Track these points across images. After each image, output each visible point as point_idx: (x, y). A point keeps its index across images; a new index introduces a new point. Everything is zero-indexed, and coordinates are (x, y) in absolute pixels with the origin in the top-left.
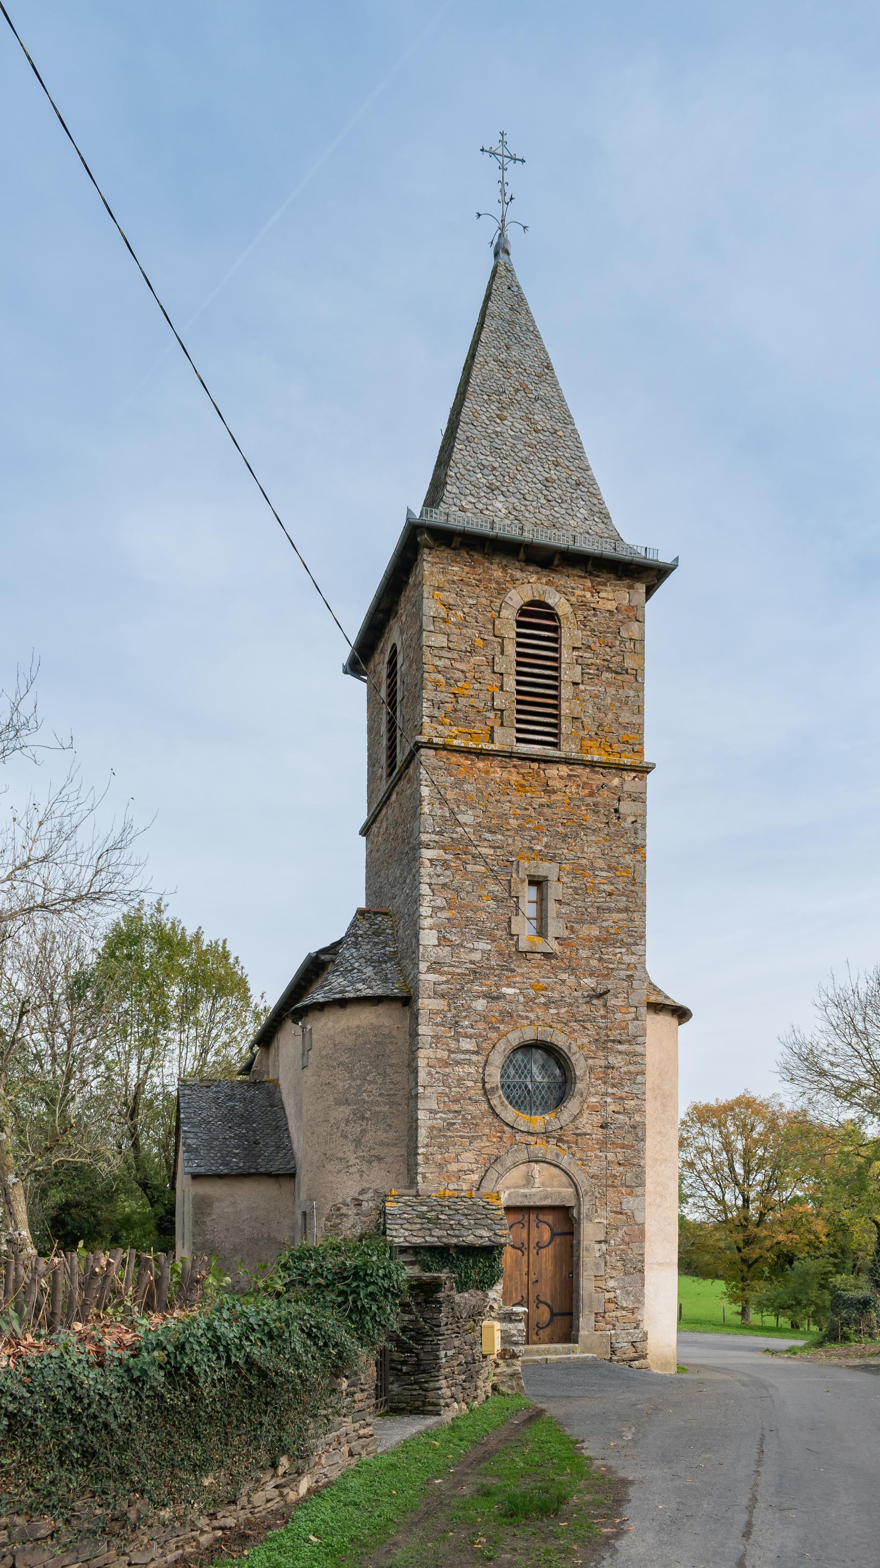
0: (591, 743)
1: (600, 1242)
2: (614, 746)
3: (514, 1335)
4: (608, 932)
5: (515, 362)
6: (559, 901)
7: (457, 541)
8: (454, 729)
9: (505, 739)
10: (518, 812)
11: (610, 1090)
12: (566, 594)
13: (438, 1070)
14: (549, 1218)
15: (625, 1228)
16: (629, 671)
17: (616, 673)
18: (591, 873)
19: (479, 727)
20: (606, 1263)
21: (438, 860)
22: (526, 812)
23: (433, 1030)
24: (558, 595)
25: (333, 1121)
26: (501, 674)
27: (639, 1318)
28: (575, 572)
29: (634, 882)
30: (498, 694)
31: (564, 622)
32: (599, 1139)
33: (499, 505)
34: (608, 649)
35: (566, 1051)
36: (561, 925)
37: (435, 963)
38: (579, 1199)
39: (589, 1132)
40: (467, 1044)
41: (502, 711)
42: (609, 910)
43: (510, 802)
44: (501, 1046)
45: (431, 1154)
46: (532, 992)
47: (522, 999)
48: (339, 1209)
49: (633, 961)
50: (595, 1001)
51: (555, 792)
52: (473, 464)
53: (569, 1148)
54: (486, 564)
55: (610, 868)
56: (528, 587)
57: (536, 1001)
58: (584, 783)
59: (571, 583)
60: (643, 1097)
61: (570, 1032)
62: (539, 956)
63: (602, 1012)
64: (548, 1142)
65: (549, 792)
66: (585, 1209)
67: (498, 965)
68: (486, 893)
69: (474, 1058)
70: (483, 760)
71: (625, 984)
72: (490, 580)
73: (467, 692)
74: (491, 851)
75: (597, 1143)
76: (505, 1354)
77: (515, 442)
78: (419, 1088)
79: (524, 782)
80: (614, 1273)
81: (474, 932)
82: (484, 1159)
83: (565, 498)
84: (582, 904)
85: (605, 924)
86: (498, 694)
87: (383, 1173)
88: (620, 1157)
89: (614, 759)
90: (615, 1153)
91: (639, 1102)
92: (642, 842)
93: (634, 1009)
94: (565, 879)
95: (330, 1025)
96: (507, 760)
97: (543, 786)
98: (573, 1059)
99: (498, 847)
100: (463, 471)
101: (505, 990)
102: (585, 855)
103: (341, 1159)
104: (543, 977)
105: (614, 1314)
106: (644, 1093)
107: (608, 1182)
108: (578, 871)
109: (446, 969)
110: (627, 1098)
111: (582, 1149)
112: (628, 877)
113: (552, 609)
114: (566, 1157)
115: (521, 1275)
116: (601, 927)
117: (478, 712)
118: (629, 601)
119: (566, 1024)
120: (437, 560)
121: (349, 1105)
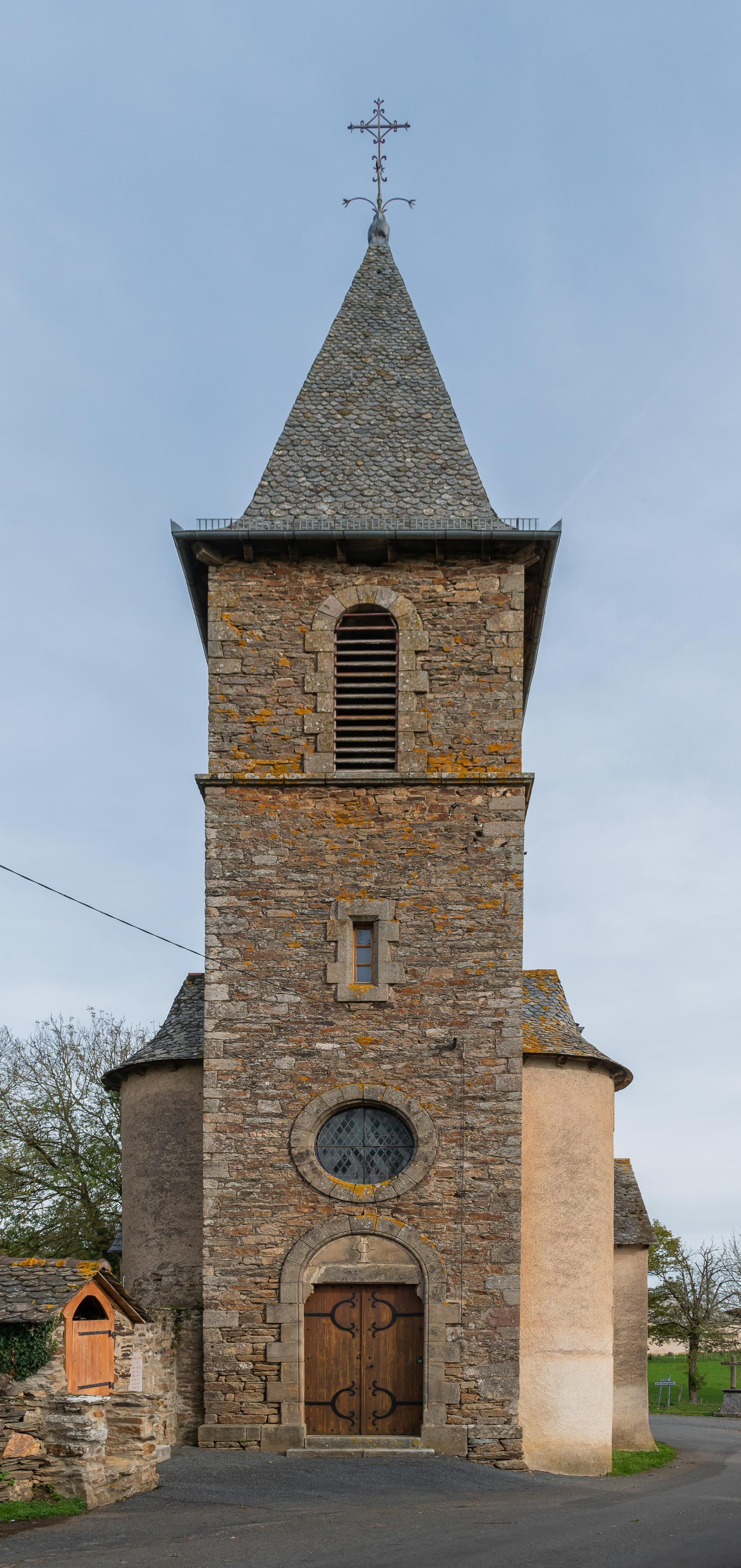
0: (443, 759)
1: (454, 1325)
2: (476, 759)
3: (70, 1430)
4: (466, 973)
5: (374, 350)
6: (395, 943)
7: (248, 551)
8: (250, 762)
9: (322, 764)
10: (338, 846)
11: (468, 1154)
12: (407, 592)
13: (230, 1135)
14: (390, 1297)
15: (490, 1310)
16: (500, 669)
17: (481, 674)
18: (441, 908)
19: (283, 757)
20: (462, 1348)
21: (228, 908)
22: (349, 846)
23: (223, 1092)
24: (394, 594)
25: (135, 1193)
26: (315, 694)
27: (511, 1412)
28: (420, 565)
29: (504, 914)
30: (309, 716)
31: (402, 624)
32: (453, 1209)
33: (325, 507)
34: (468, 649)
35: (404, 1111)
36: (398, 969)
37: (225, 1019)
38: (423, 1276)
39: (439, 1201)
40: (265, 1107)
41: (316, 735)
42: (468, 948)
43: (326, 836)
44: (313, 1107)
45: (221, 1226)
46: (357, 1047)
47: (343, 1055)
48: (140, 1284)
49: (502, 1005)
50: (446, 1054)
51: (389, 820)
52: (296, 468)
53: (410, 1219)
54: (294, 573)
55: (469, 900)
56: (352, 590)
57: (363, 1056)
58: (432, 806)
59: (413, 577)
60: (518, 1161)
61: (411, 1089)
62: (367, 1006)
63: (457, 1065)
64: (379, 1212)
65: (382, 820)
66: (430, 1287)
67: (310, 1018)
68: (294, 939)
69: (278, 1121)
70: (289, 793)
71: (491, 1032)
72: (299, 591)
73: (267, 719)
74: (302, 893)
75: (450, 1214)
76: (59, 1451)
77: (357, 435)
78: (205, 1155)
79: (345, 812)
80: (474, 1361)
81: (278, 983)
82: (291, 1231)
83: (420, 486)
84: (429, 944)
85: (462, 965)
86: (309, 716)
87: (184, 1247)
88: (484, 1230)
89: (476, 774)
90: (476, 1225)
91: (511, 1167)
92: (518, 868)
93: (504, 1061)
94: (403, 917)
95: (132, 1094)
96: (323, 790)
97: (373, 814)
98: (414, 1120)
99: (310, 888)
100: (280, 478)
101: (319, 1045)
102: (433, 888)
103: (141, 1232)
104: (373, 1029)
105: (474, 1406)
106: (519, 1157)
107: (465, 1257)
108: (421, 905)
109: (239, 1025)
110: (493, 1162)
111: (428, 1221)
112: (495, 909)
113: (387, 611)
114: (403, 1229)
115: (351, 1358)
116: (455, 970)
117: (285, 740)
118: (500, 587)
119: (405, 1081)
120: (227, 577)
121: (148, 1176)
